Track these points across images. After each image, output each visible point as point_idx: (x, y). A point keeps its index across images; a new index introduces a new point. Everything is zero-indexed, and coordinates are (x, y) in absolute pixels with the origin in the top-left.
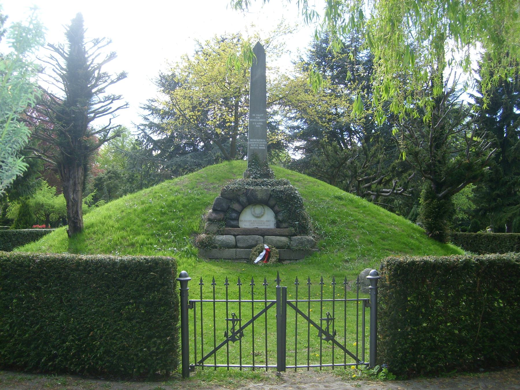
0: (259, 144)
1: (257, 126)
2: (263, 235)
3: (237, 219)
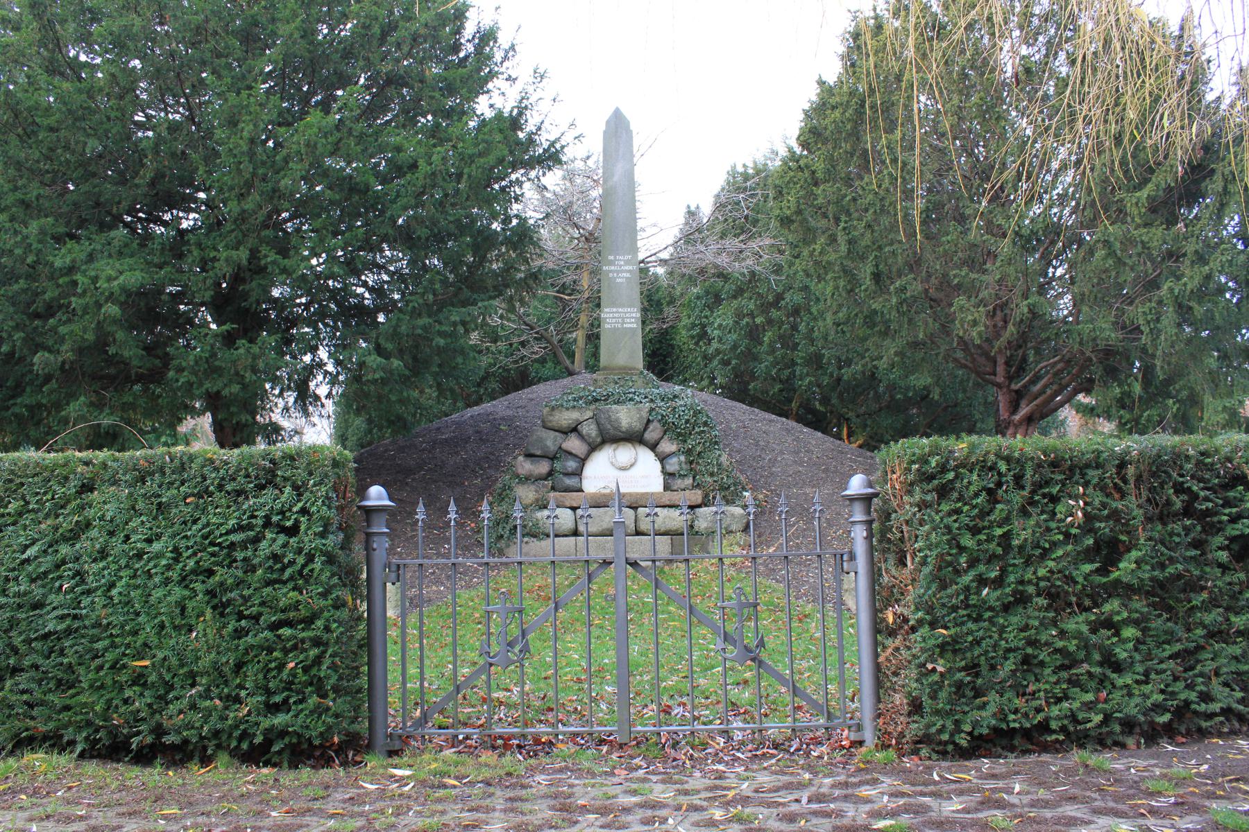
0: (623, 319)
1: (618, 280)
3: (578, 473)
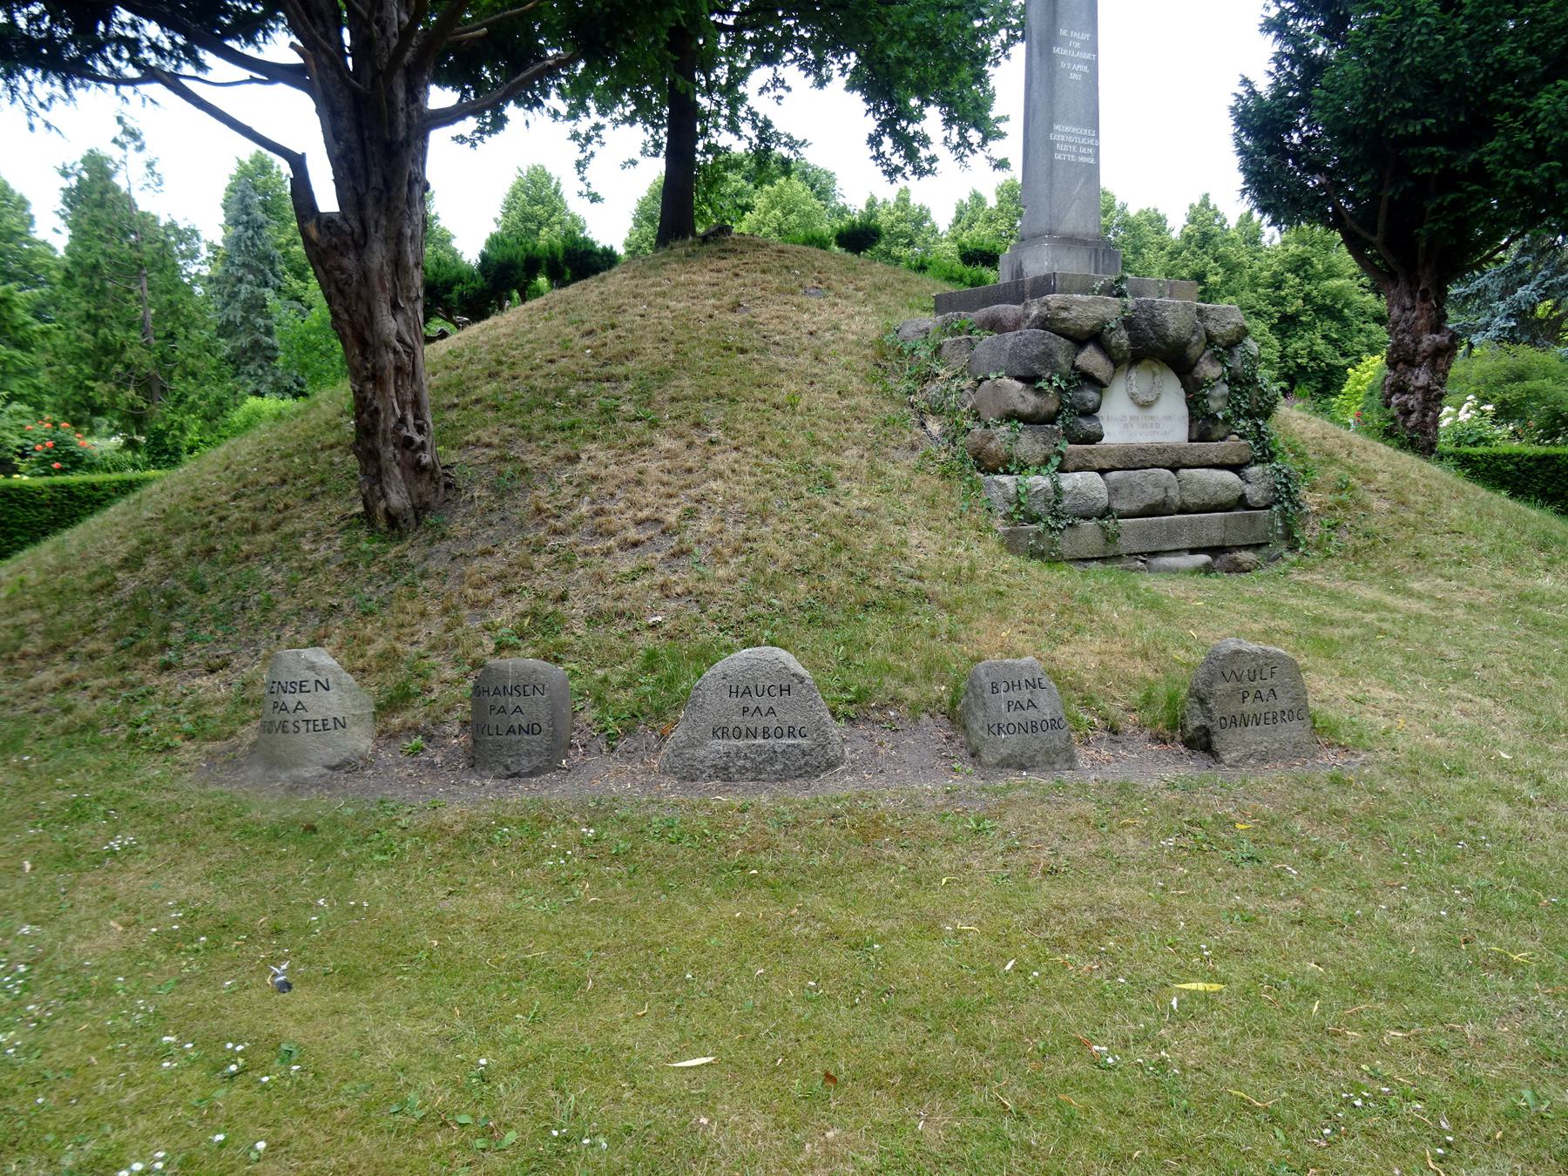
0: (1078, 146)
1: (1074, 76)
2: (1174, 469)
3: (1090, 413)
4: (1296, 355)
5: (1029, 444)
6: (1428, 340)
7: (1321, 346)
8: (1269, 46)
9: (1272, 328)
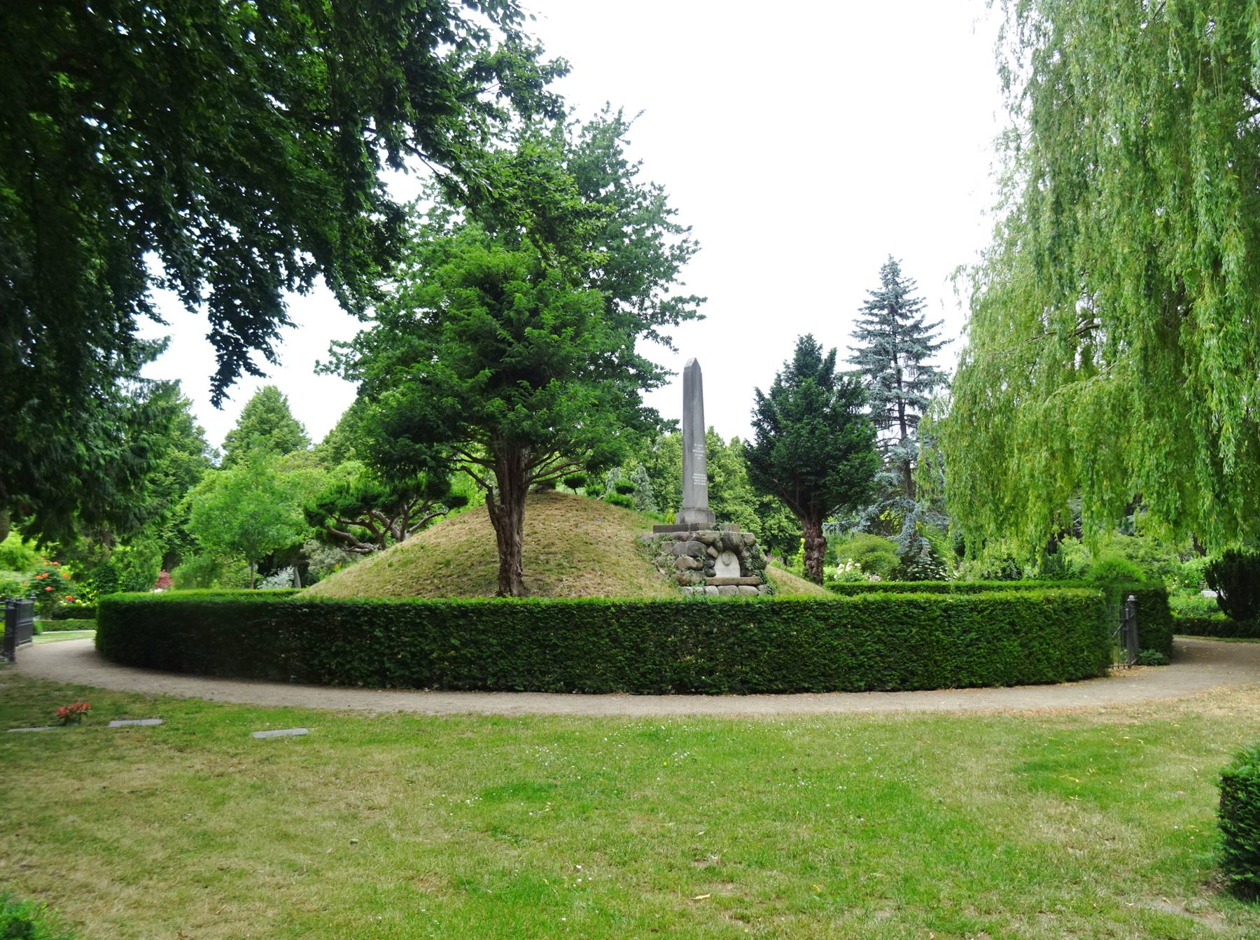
3: (712, 567)
4: (771, 528)
5: (695, 577)
6: (817, 541)
7: (785, 523)
8: (755, 430)
9: (756, 510)
